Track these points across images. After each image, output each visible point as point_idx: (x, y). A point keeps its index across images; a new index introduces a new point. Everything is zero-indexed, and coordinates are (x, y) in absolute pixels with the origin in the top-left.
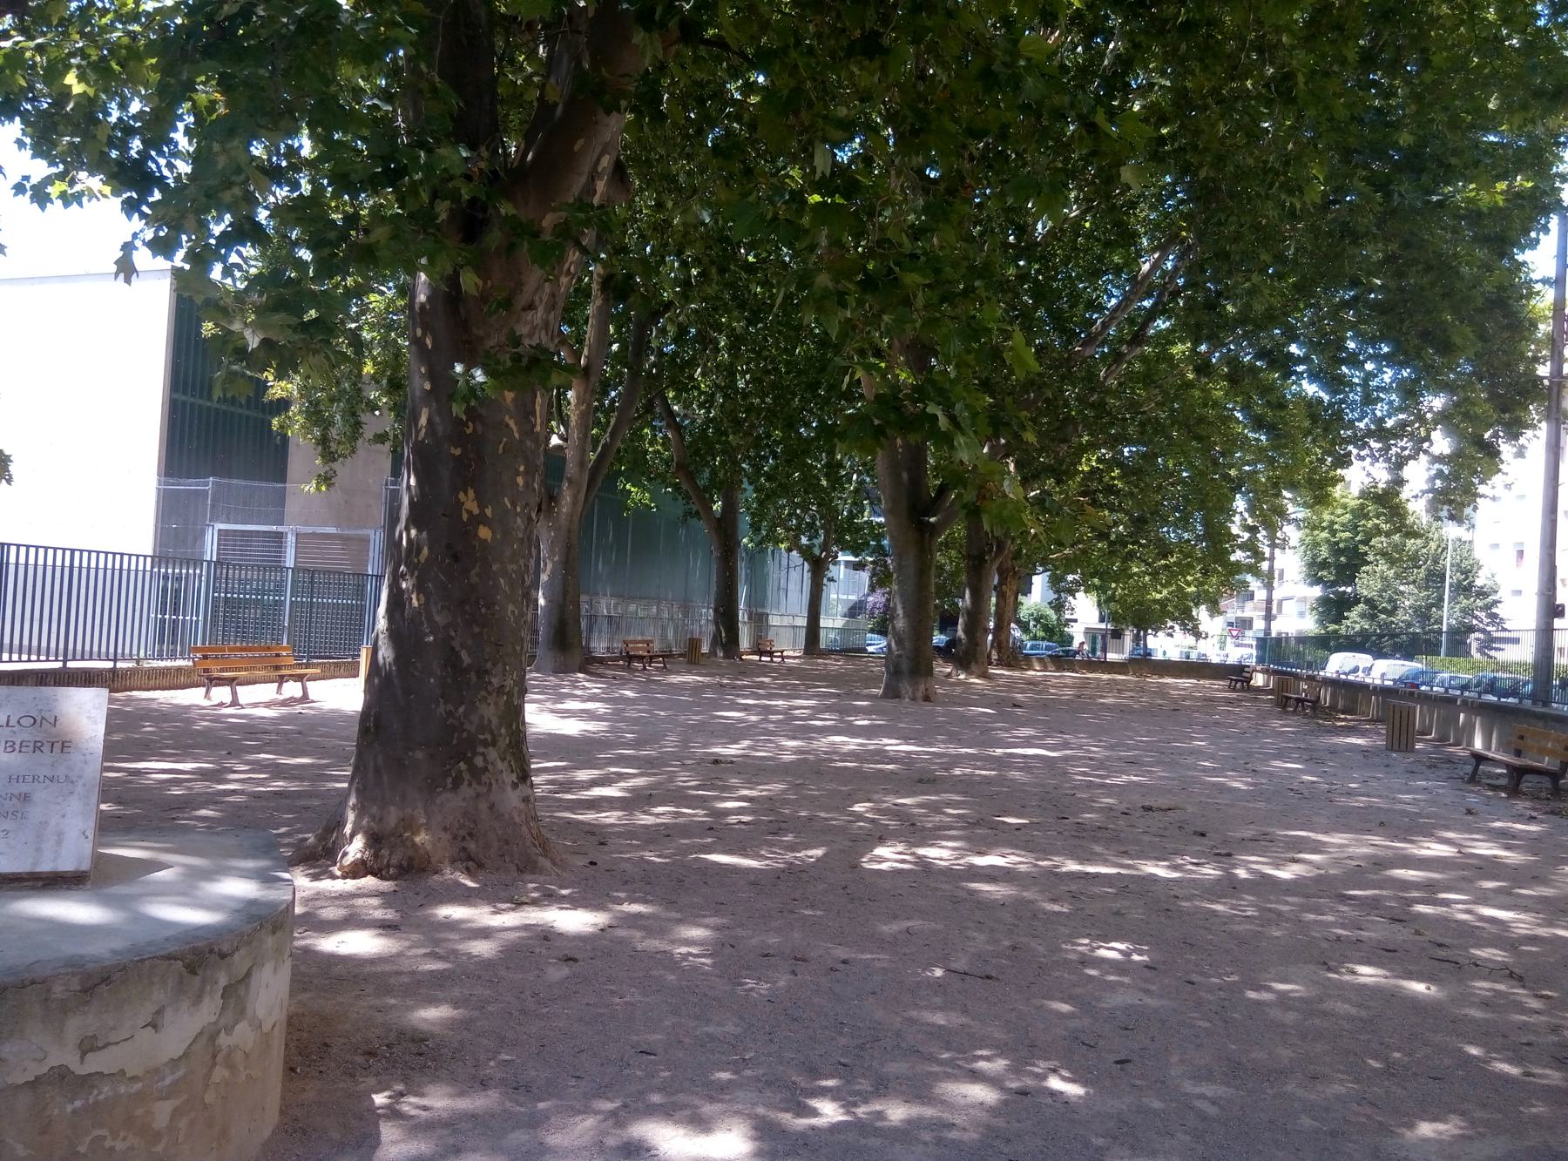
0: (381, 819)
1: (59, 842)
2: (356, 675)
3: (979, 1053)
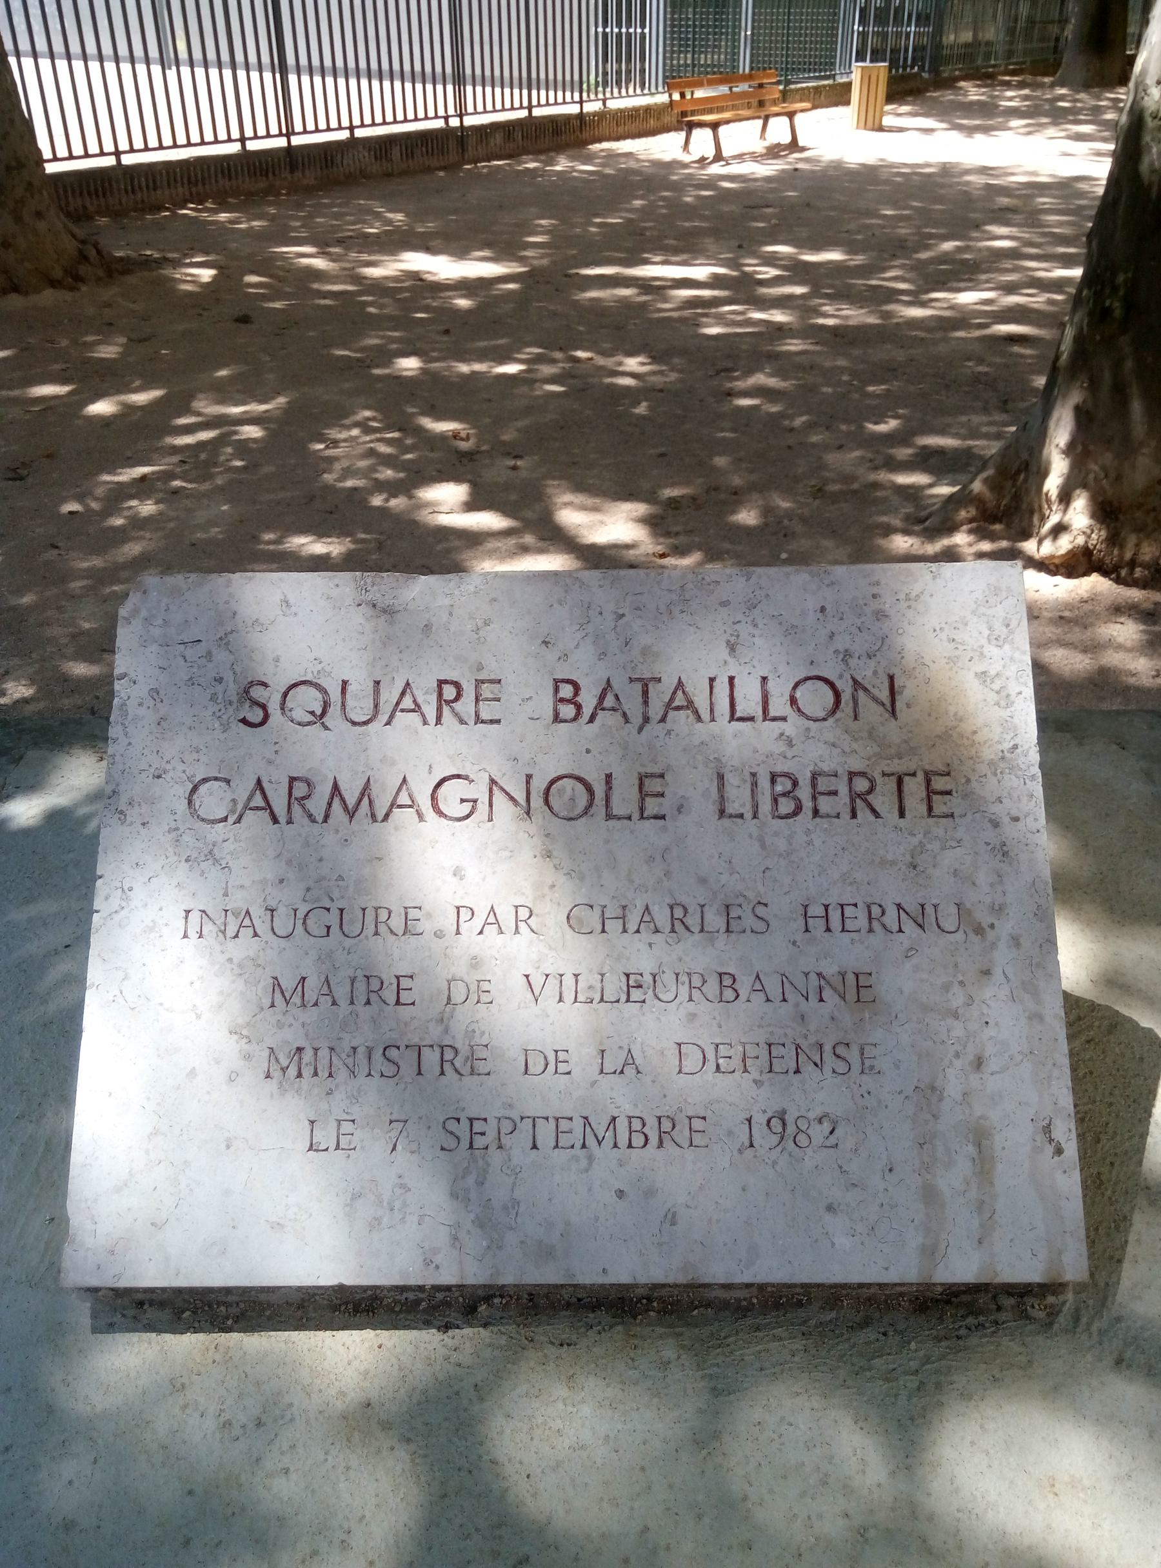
0: (1119, 478)
1: (984, 1164)
2: (847, 103)
3: (900, 224)
